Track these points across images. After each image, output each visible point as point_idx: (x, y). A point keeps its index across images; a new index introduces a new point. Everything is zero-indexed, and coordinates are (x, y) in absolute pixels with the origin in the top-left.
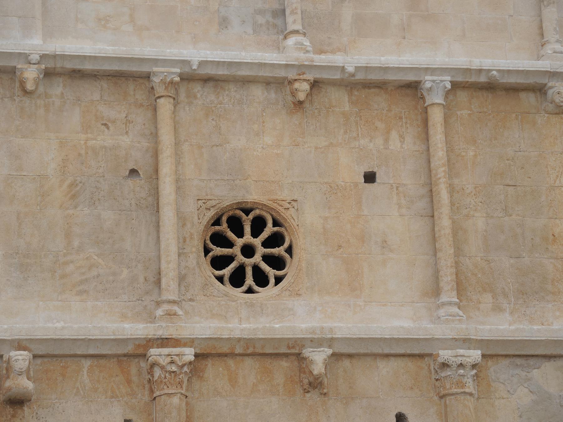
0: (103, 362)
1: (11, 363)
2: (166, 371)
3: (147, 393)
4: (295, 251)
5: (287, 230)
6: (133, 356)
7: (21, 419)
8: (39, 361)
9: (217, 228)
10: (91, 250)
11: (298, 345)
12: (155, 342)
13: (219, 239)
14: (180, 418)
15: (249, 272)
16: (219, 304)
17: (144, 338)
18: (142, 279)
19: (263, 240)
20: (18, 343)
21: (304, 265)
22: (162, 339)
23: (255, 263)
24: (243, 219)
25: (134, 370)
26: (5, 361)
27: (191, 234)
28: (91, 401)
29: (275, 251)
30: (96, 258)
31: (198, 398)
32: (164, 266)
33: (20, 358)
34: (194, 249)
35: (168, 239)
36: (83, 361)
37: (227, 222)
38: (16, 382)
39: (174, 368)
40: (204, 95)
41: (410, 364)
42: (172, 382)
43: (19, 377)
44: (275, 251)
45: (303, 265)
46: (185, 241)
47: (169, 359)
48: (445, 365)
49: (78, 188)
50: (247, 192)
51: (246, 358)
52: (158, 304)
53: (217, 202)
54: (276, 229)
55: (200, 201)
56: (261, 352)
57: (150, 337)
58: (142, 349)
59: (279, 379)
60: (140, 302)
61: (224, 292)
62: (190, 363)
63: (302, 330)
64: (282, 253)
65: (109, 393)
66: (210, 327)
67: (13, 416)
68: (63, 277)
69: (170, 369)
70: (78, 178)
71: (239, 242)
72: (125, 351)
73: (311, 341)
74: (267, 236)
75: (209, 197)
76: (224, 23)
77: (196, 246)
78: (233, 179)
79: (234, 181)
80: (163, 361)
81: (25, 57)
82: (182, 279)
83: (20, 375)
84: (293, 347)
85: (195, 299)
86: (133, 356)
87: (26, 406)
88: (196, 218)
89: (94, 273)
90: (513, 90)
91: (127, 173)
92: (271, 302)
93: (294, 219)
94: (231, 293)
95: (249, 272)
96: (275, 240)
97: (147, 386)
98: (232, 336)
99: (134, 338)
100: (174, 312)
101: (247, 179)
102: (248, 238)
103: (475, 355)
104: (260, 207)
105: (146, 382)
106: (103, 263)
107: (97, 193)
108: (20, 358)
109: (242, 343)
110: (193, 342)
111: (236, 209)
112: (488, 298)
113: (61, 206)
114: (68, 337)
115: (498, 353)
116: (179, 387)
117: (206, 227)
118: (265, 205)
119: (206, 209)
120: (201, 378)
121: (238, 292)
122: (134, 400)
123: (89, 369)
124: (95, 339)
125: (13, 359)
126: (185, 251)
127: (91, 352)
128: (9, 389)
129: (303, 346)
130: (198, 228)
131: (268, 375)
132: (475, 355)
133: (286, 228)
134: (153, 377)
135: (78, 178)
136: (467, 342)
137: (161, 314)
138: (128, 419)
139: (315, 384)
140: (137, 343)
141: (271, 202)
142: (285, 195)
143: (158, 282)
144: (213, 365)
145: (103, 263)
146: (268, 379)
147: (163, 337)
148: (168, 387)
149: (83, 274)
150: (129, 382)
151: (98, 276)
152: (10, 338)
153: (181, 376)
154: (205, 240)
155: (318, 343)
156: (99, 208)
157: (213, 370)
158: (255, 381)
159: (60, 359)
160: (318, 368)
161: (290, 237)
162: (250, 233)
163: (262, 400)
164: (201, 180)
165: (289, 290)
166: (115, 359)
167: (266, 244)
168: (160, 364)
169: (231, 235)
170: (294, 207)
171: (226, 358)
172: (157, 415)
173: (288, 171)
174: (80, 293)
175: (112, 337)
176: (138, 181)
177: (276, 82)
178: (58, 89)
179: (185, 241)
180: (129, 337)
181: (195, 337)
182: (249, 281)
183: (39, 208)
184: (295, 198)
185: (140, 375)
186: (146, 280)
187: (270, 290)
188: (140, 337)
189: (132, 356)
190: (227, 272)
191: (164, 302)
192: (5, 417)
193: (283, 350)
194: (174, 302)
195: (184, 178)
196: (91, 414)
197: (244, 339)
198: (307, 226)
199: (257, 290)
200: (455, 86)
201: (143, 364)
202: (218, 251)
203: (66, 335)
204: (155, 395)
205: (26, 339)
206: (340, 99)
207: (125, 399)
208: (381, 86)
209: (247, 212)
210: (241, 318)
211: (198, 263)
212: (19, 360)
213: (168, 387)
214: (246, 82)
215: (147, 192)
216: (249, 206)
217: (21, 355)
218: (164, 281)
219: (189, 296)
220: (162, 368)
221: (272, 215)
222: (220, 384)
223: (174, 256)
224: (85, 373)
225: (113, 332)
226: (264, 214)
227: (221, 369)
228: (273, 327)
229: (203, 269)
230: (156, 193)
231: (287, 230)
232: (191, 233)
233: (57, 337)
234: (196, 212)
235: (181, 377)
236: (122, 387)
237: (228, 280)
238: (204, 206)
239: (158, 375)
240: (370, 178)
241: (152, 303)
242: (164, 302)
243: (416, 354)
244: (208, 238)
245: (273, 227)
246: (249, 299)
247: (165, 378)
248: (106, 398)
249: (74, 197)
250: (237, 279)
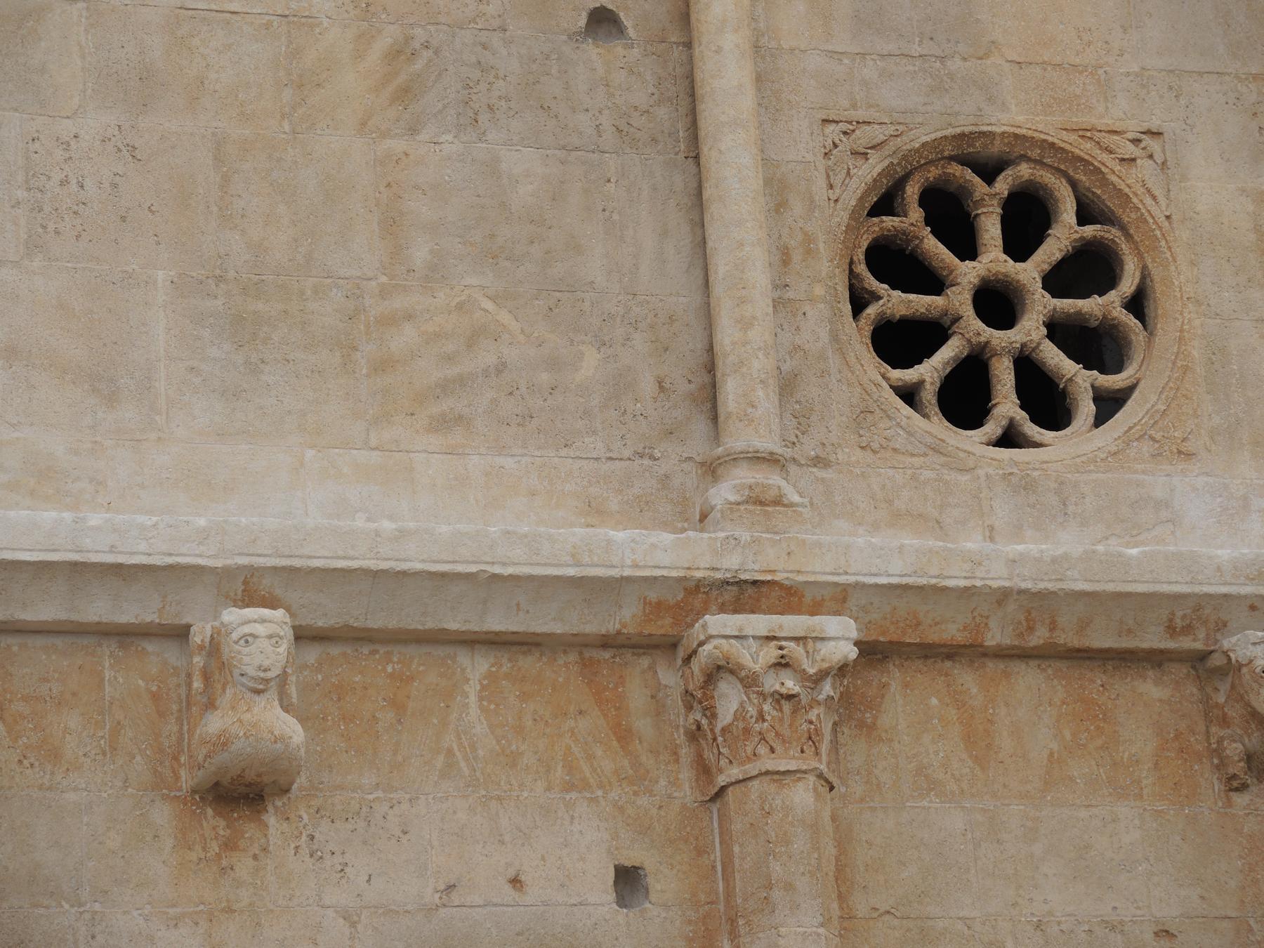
0: (529, 663)
1: (225, 651)
2: (761, 694)
3: (686, 774)
4: (1163, 304)
5: (1128, 236)
6: (634, 647)
7: (255, 857)
8: (312, 654)
9: (889, 222)
10: (473, 281)
11: (1205, 622)
12: (715, 593)
14: (819, 859)
15: (1004, 377)
16: (914, 477)
17: (680, 580)
18: (647, 386)
19: (1047, 267)
20: (245, 583)
21: (1196, 351)
22: (740, 583)
23: (1023, 345)
24: (977, 196)
25: (636, 695)
26: (201, 648)
27: (808, 239)
28: (499, 799)
29: (1091, 306)
30: (489, 305)
31: (862, 800)
32: (727, 335)
33: (260, 629)
34: (819, 290)
35: (741, 245)
36: (463, 658)
37: (922, 203)
38: (247, 716)
39: (791, 684)
42: (786, 732)
43: (257, 698)
44: (1091, 306)
45: (1195, 353)
46: (786, 259)
47: (770, 653)
49: (419, 65)
50: (991, 100)
51: (1019, 667)
52: (712, 470)
53: (891, 130)
54: (1089, 231)
55: (832, 127)
56: (1076, 642)
57: (699, 574)
58: (668, 621)
59: (1138, 740)
60: (646, 462)
61: (929, 440)
62: (843, 670)
63: (1219, 569)
64: (1115, 314)
65: (559, 772)
66: (901, 548)
67: (230, 845)
68: (382, 365)
69: (777, 687)
70: (418, 31)
71: (968, 273)
72: (611, 626)
73: (1253, 608)
74: (1058, 256)
75: (861, 114)
77: (824, 279)
78: (939, 53)
79: (942, 59)
80: (755, 658)
82: (787, 386)
83: (259, 692)
84: (1188, 629)
85: (832, 458)
86: (634, 647)
87: (270, 808)
88: (822, 182)
89: (487, 357)
91: (583, 22)
92: (1094, 476)
93: (1154, 198)
94: (952, 442)
95: (1004, 377)
96: (1087, 269)
97: (686, 752)
98: (978, 583)
99: (645, 579)
100: (772, 494)
101: (987, 55)
102: (993, 258)
104: (1035, 154)
105: (681, 738)
106: (514, 326)
107: (483, 87)
108: (260, 629)
109: (1011, 607)
110: (844, 600)
111: (952, 158)
113: (364, 124)
114: (419, 566)
116: (810, 751)
117: (854, 215)
118: (1053, 145)
119: (855, 153)
120: (868, 729)
121: (972, 442)
122: (643, 801)
123: (483, 688)
124: (512, 577)
125: (235, 636)
126: (790, 294)
127: (496, 623)
128: (223, 742)
129: (1222, 626)
131: (1098, 728)
133: (1123, 228)
134: (714, 716)
135: (418, 31)
137: (732, 498)
138: (628, 863)
140: (653, 596)
141: (1072, 137)
142: (1120, 112)
143: (709, 398)
144: (906, 685)
145: (514, 326)
146: (1099, 742)
147: (743, 577)
148: (772, 750)
149: (450, 359)
150: (624, 735)
151: (501, 368)
152: (219, 563)
153: (816, 711)
154: (851, 263)
156: (490, 136)
158: (1055, 746)
159: (382, 650)
161: (1140, 256)
162: (999, 242)
163: (1083, 813)
164: (831, 54)
165: (1152, 438)
166: (572, 657)
167: (1056, 282)
168: (741, 667)
169: (935, 249)
170: (1151, 157)
171: (948, 664)
172: (736, 849)
173: (1125, 31)
174: (442, 424)
175: (571, 572)
176: (620, 50)
179: (786, 259)
180: (627, 573)
181: (852, 579)
182: (1007, 405)
183: (287, 128)
184: (1154, 125)
185: (658, 714)
186: (661, 388)
188: (665, 573)
189: (632, 650)
190: (930, 371)
191: (734, 459)
192: (198, 848)
193: (1153, 639)
194: (771, 460)
195: (773, 44)
196: (502, 842)
197: (1021, 592)
199: (1037, 438)
201: (669, 677)
202: (897, 303)
203: (415, 557)
204: (721, 780)
205: (275, 569)
207: (614, 795)
209: (989, 172)
210: (992, 528)
211: (835, 338)
212: (255, 636)
213: (772, 750)
215: (651, 89)
216: (996, 148)
217: (263, 621)
218: (731, 390)
219: (809, 448)
220: (749, 682)
221: (1074, 184)
222: (936, 753)
223: (761, 305)
224: (473, 699)
225: (573, 556)
226: (1048, 178)
227: (934, 701)
228: (1120, 555)
229: (852, 358)
231: (1128, 236)
232: (806, 234)
233: (384, 565)
234: (821, 163)
235: (813, 715)
236: (599, 753)
237: (934, 401)
238: (846, 144)
239: (734, 706)
241: (687, 466)
242: (734, 459)
244: (860, 255)
246: (1016, 464)
247: (761, 717)
248: (548, 789)
249: (405, 94)
250: (964, 400)
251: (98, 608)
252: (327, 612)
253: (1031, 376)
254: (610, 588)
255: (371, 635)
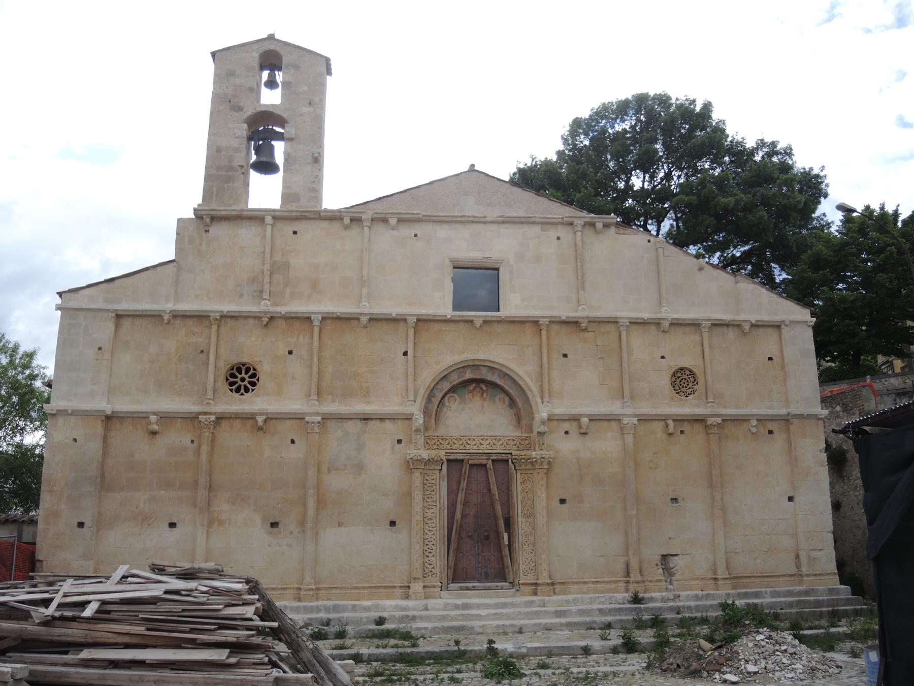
13: (233, 376)
40: (231, 323)
41: (298, 421)
48: (308, 423)
71: (240, 376)
76: (241, 295)
81: (164, 311)
82: (215, 391)
90: (348, 319)
102: (240, 376)
103: (319, 418)
112: (330, 397)
115: (327, 418)
130: (224, 369)
132: (319, 418)
136: (317, 414)
139: (260, 429)
142: (257, 359)
155: (261, 414)
157: (224, 423)
160: (260, 423)
177: (257, 317)
178: (178, 321)
187: (249, 394)
189: (192, 418)
198: (265, 370)
200: (323, 318)
206: (282, 324)
208: (297, 318)
214: (247, 317)
230: (208, 359)
240: (290, 352)
243: (299, 418)
245: (454, 310)
250: (238, 390)
251: (141, 415)
252: (163, 415)
253: (246, 387)
254: (191, 413)
255: (167, 418)
